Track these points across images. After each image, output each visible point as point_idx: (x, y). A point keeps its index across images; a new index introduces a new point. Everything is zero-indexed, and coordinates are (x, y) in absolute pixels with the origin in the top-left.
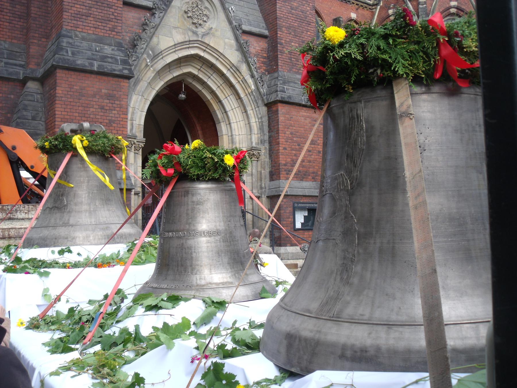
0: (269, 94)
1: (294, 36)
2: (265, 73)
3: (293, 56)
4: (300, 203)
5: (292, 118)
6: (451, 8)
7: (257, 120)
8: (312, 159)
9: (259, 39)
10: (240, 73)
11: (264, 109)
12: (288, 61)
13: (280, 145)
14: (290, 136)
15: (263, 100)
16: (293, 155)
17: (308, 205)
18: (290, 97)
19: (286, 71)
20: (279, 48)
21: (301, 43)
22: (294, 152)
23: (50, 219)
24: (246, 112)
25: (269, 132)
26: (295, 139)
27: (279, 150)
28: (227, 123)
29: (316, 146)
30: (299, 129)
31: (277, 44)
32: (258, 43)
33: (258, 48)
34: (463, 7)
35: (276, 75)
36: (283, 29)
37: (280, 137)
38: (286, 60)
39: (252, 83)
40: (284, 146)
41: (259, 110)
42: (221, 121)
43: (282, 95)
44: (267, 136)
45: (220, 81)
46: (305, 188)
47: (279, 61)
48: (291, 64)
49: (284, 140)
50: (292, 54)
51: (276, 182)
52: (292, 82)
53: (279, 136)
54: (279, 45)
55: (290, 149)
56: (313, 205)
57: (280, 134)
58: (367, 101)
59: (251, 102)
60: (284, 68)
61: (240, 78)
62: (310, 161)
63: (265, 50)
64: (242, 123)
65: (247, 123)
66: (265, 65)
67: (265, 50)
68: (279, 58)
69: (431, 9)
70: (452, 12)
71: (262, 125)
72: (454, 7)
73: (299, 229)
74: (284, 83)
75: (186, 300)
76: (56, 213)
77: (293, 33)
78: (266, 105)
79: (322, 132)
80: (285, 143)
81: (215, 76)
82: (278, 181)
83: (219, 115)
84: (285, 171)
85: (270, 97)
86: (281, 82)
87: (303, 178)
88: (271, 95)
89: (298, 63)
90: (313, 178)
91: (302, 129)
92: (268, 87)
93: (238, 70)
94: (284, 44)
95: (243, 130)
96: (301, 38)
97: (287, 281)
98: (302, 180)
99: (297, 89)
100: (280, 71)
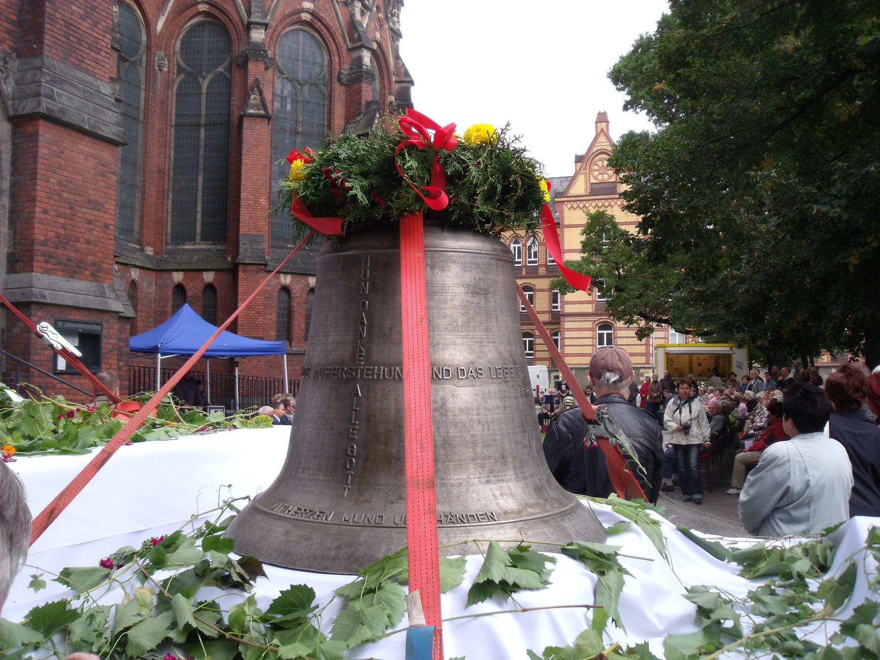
0: (20, 97)
2: (11, 54)
3: (72, 33)
4: (68, 321)
5: (62, 152)
6: (304, 11)
8: (93, 238)
12: (63, 39)
13: (38, 204)
14: (57, 187)
16: (60, 225)
17: (81, 326)
18: (62, 111)
19: (58, 59)
20: (48, 10)
21: (89, 10)
22: (62, 220)
25: (13, 174)
26: (65, 195)
27: (34, 212)
29: (101, 214)
30: (73, 176)
34: (322, 14)
35: (37, 62)
37: (38, 188)
38: (59, 37)
40: (44, 206)
43: (49, 106)
44: (8, 182)
46: (78, 292)
47: (46, 36)
48: (68, 48)
49: (44, 195)
50: (72, 28)
51: (21, 278)
52: (67, 82)
53: (35, 184)
55: (53, 213)
56: (90, 327)
57: (39, 182)
60: (54, 51)
62: (88, 242)
69: (270, 6)
70: (304, 19)
72: (307, 11)
73: (62, 373)
74: (54, 81)
78: (10, 119)
80: (46, 200)
82: (27, 274)
84: (44, 255)
85: (23, 105)
86: (48, 78)
87: (75, 272)
89: (81, 48)
90: (93, 275)
91: (80, 178)
92: (17, 84)
98: (72, 277)
99: (77, 99)
100: (47, 56)
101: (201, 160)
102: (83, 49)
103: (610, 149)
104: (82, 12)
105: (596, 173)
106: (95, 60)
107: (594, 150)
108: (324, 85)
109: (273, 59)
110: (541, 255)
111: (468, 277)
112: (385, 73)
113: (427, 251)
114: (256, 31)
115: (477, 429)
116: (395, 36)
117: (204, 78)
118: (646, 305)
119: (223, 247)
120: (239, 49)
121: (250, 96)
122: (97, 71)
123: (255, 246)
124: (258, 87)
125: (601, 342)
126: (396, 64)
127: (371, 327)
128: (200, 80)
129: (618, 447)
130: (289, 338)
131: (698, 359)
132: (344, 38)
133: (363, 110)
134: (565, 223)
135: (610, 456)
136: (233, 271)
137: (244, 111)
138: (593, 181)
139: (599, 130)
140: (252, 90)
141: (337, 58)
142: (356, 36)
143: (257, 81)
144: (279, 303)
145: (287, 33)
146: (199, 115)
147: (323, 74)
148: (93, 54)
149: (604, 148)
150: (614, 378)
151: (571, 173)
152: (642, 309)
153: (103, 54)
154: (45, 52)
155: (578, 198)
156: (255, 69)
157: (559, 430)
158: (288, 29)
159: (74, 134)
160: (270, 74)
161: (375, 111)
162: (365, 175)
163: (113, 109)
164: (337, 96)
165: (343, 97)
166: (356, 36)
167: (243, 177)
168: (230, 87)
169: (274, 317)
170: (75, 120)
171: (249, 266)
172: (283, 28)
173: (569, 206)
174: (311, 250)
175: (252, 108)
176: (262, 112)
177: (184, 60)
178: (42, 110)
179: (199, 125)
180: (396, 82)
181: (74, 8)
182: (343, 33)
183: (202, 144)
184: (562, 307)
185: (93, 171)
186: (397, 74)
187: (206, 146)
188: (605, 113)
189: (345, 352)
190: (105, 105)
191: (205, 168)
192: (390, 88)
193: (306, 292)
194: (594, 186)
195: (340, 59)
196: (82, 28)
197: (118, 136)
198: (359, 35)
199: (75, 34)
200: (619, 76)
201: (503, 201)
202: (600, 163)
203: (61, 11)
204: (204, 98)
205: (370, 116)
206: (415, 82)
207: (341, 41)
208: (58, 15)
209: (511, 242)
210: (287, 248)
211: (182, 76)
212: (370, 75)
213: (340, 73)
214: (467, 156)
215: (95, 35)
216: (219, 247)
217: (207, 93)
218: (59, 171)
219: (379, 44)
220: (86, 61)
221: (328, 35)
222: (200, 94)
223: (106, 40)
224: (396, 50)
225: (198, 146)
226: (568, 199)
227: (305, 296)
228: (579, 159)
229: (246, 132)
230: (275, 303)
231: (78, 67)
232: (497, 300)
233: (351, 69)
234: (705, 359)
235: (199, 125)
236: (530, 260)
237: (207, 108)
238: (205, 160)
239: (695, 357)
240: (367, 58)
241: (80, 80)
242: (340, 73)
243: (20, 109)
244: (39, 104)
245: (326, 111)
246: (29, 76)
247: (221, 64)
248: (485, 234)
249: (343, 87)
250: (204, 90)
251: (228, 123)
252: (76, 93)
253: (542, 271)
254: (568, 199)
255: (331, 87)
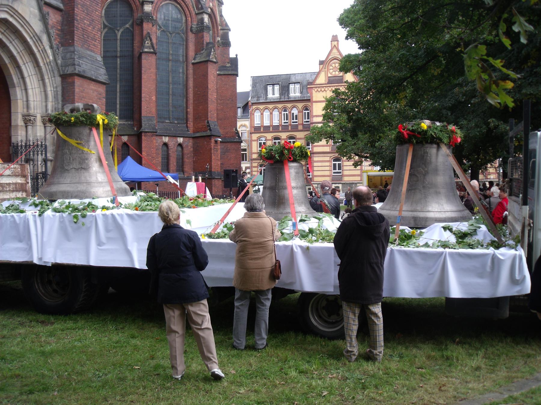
1: (87, 15)
3: (85, 33)
7: (52, 89)
9: (55, 11)
10: (42, 43)
11: (59, 80)
12: (82, 37)
15: (59, 71)
18: (84, 71)
19: (80, 46)
20: (75, 24)
23: (80, 177)
24: (43, 79)
28: (23, 88)
31: (74, 20)
32: (54, 15)
33: (54, 20)
35: (71, 49)
36: (79, 6)
38: (80, 36)
39: (51, 54)
41: (55, 80)
42: (16, 85)
43: (79, 69)
45: (21, 48)
47: (75, 37)
54: (75, 22)
58: (430, 148)
59: (48, 71)
60: (78, 43)
61: (40, 47)
63: (59, 23)
64: (37, 90)
65: (42, 90)
66: (59, 38)
67: (59, 23)
68: (75, 34)
71: (57, 94)
74: (79, 58)
75: (242, 218)
76: (84, 173)
77: (86, 11)
78: (61, 76)
79: (105, 105)
81: (16, 42)
83: (15, 79)
85: (67, 69)
88: (67, 67)
92: (62, 59)
93: (40, 40)
94: (79, 21)
95: (38, 97)
96: (91, 17)
97: (192, 223)
100: (76, 46)
101: (118, 76)
102: (89, 40)
103: (339, 57)
104: (88, 23)
105: (331, 71)
106: (94, 45)
107: (330, 57)
108: (183, 34)
109: (156, 20)
110: (300, 118)
111: (296, 170)
112: (215, 24)
113: (287, 165)
114: (147, 5)
115: (298, 198)
116: (220, 4)
117: (118, 31)
118: (358, 149)
119: (132, 123)
120: (137, 15)
121: (145, 41)
122: (95, 50)
123: (150, 123)
124: (150, 37)
125: (335, 169)
126: (221, 19)
127: (278, 180)
128: (116, 32)
129: (324, 203)
130: (183, 171)
131: (385, 178)
132: (193, 7)
133: (205, 47)
134: (314, 100)
135: (323, 205)
136: (138, 136)
137: (142, 50)
138: (329, 75)
139: (333, 46)
140: (146, 39)
141: (190, 18)
142: (200, 6)
143: (148, 33)
144: (162, 152)
145: (163, 5)
146: (116, 51)
147: (182, 28)
148: (93, 42)
149: (336, 56)
150: (328, 188)
151: (317, 70)
152: (356, 151)
153: (97, 41)
154: (75, 44)
155: (321, 86)
156: (147, 27)
157: (313, 202)
158: (163, 3)
159: (88, 81)
160: (154, 28)
161: (211, 48)
162: (278, 153)
163: (103, 67)
164: (190, 40)
165: (193, 40)
166: (200, 6)
167: (143, 86)
168: (133, 36)
169: (160, 159)
170: (88, 75)
171: (148, 133)
172: (161, 3)
173: (316, 90)
174: (178, 123)
175: (146, 48)
176: (152, 50)
177: (107, 21)
178: (76, 72)
179: (116, 57)
180: (221, 29)
181: (85, 21)
182: (193, 5)
183: (119, 67)
184: (312, 148)
185: (96, 98)
186: (221, 26)
187: (121, 68)
188: (336, 36)
189: (274, 184)
190: (100, 66)
191: (120, 80)
192: (218, 33)
193: (176, 146)
194: (330, 79)
195: (191, 19)
196: (89, 31)
197: (106, 80)
198: (202, 6)
199: (87, 34)
200: (343, 21)
201: (302, 156)
202: (333, 65)
203: (81, 24)
204: (118, 42)
205: (209, 51)
206: (231, 30)
207: (192, 9)
208: (79, 26)
209: (282, 110)
210: (166, 122)
211: (106, 30)
212: (208, 27)
213: (191, 27)
214: (295, 150)
215: (94, 33)
216: (129, 123)
217: (120, 39)
218: (83, 99)
219: (212, 9)
220: (91, 46)
221: (185, 6)
222: (116, 39)
223: (98, 35)
224: (220, 12)
225: (116, 68)
226: (315, 86)
227: (176, 148)
228: (321, 63)
229: (144, 62)
230: (160, 151)
231: (87, 49)
232: (300, 174)
233: (197, 25)
234: (389, 179)
235: (116, 57)
236: (293, 121)
237: (120, 47)
238: (120, 75)
239: (383, 178)
240: (206, 18)
241: (90, 56)
242: (191, 27)
243: (66, 71)
244: (75, 69)
245: (184, 48)
246: (68, 55)
247: (127, 23)
248: (298, 162)
249: (194, 35)
250: (119, 37)
251: (132, 56)
252: (88, 62)
253: (300, 127)
254: (315, 86)
255: (187, 35)
